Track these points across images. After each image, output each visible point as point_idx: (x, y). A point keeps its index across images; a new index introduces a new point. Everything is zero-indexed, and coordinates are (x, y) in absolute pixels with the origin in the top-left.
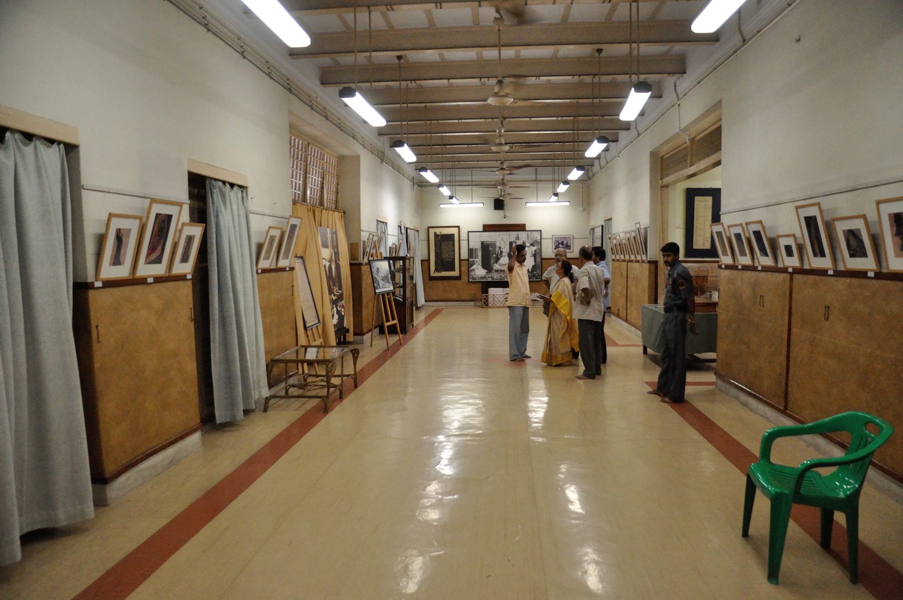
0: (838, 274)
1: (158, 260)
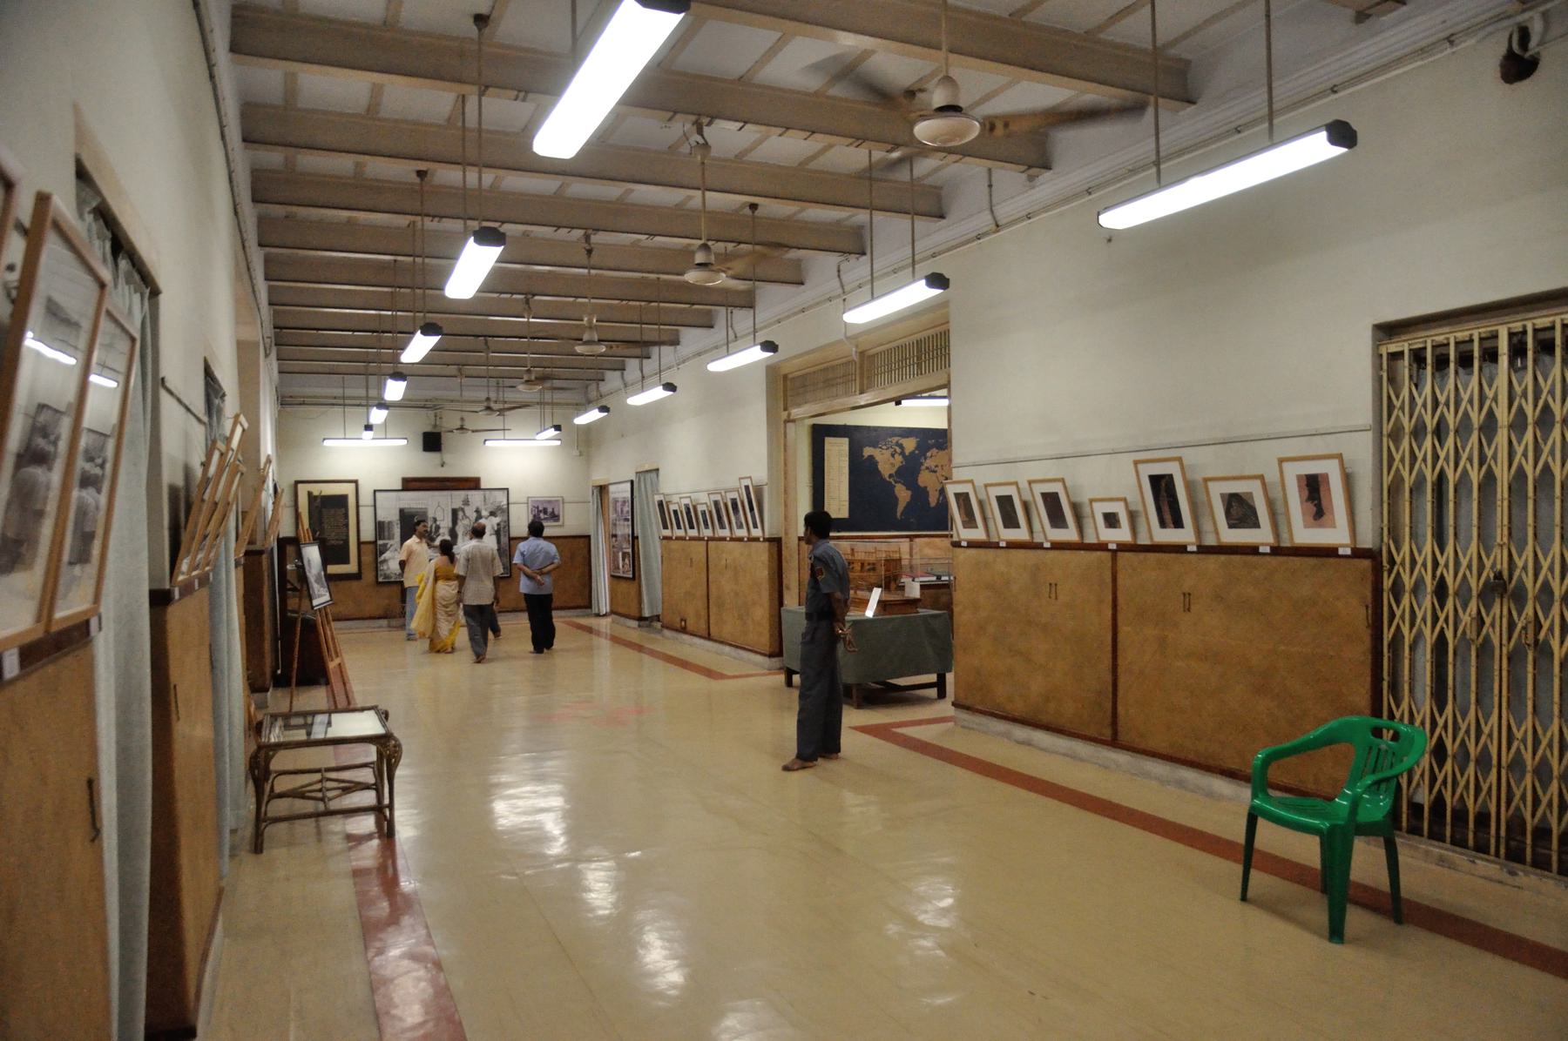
0: (1204, 550)
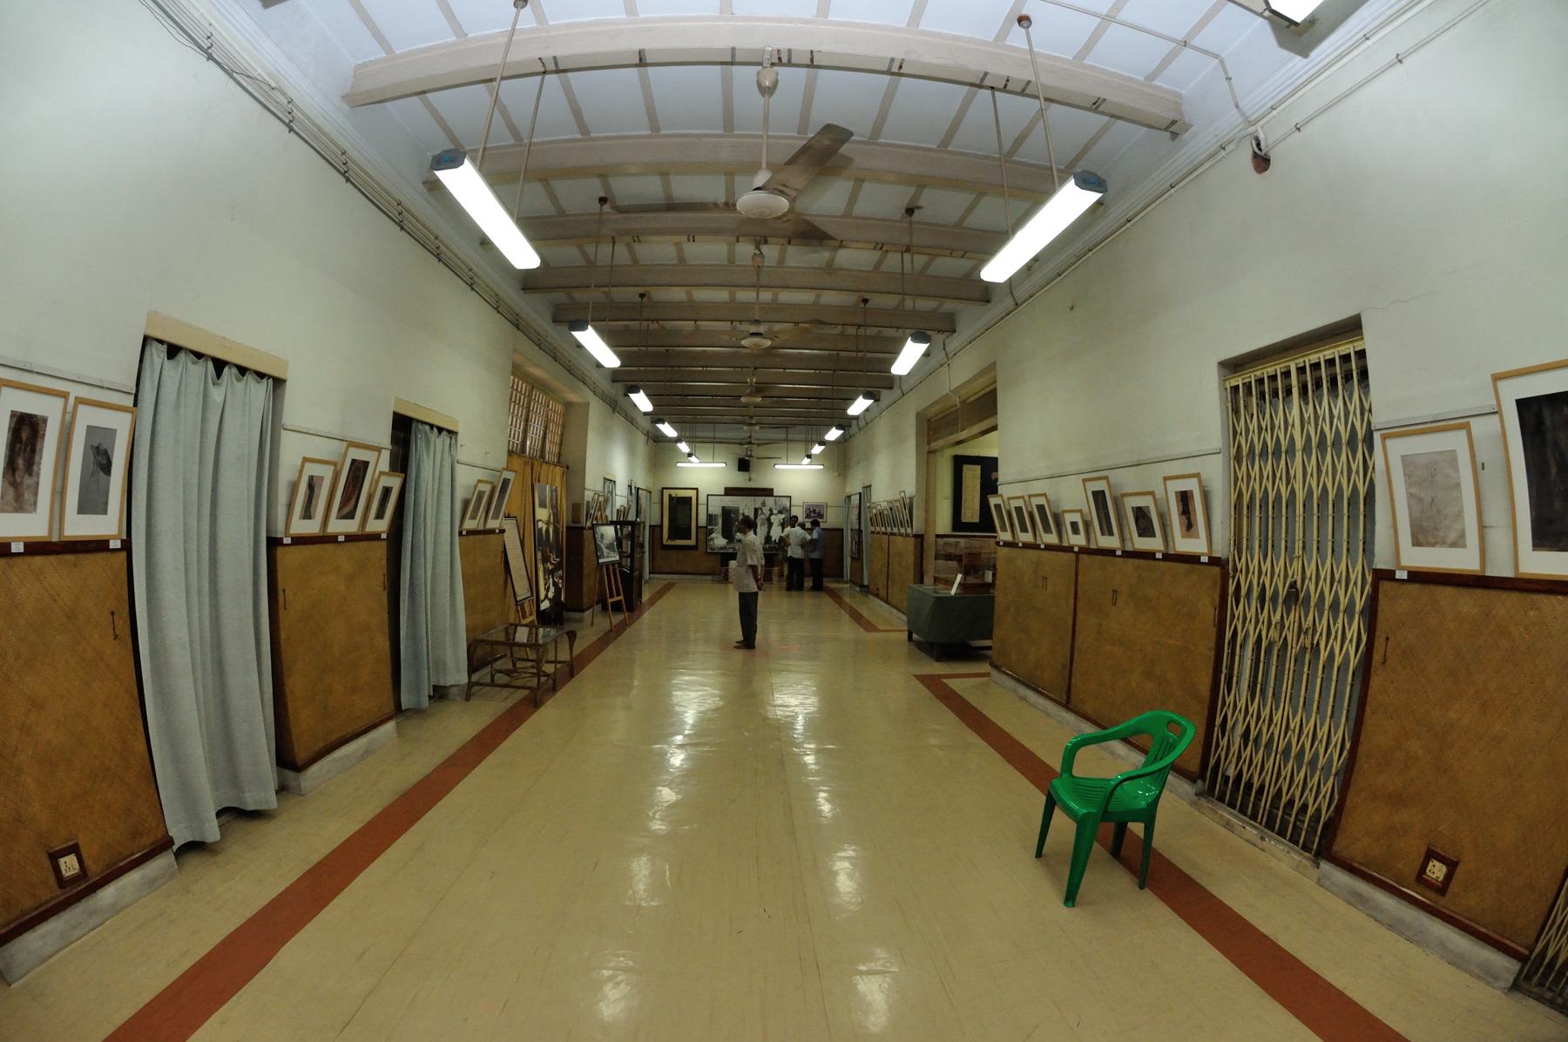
0: (1128, 555)
1: (351, 516)
